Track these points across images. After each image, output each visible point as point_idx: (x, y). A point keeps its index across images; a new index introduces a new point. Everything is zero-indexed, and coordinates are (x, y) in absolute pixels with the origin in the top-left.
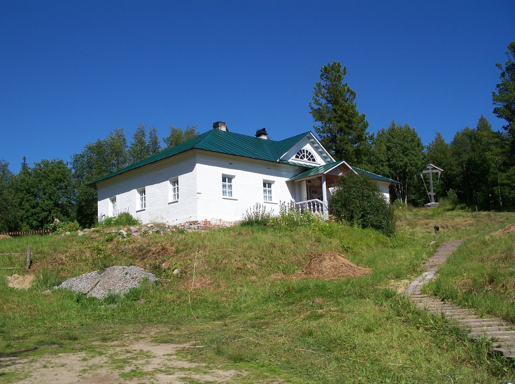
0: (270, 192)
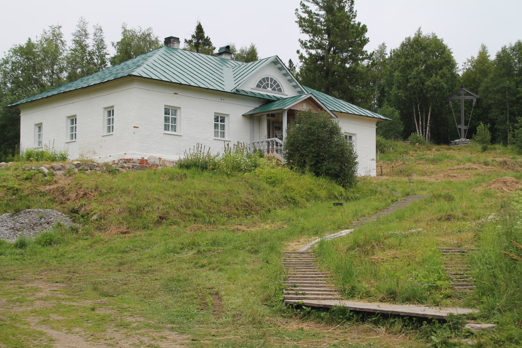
0: (223, 127)
